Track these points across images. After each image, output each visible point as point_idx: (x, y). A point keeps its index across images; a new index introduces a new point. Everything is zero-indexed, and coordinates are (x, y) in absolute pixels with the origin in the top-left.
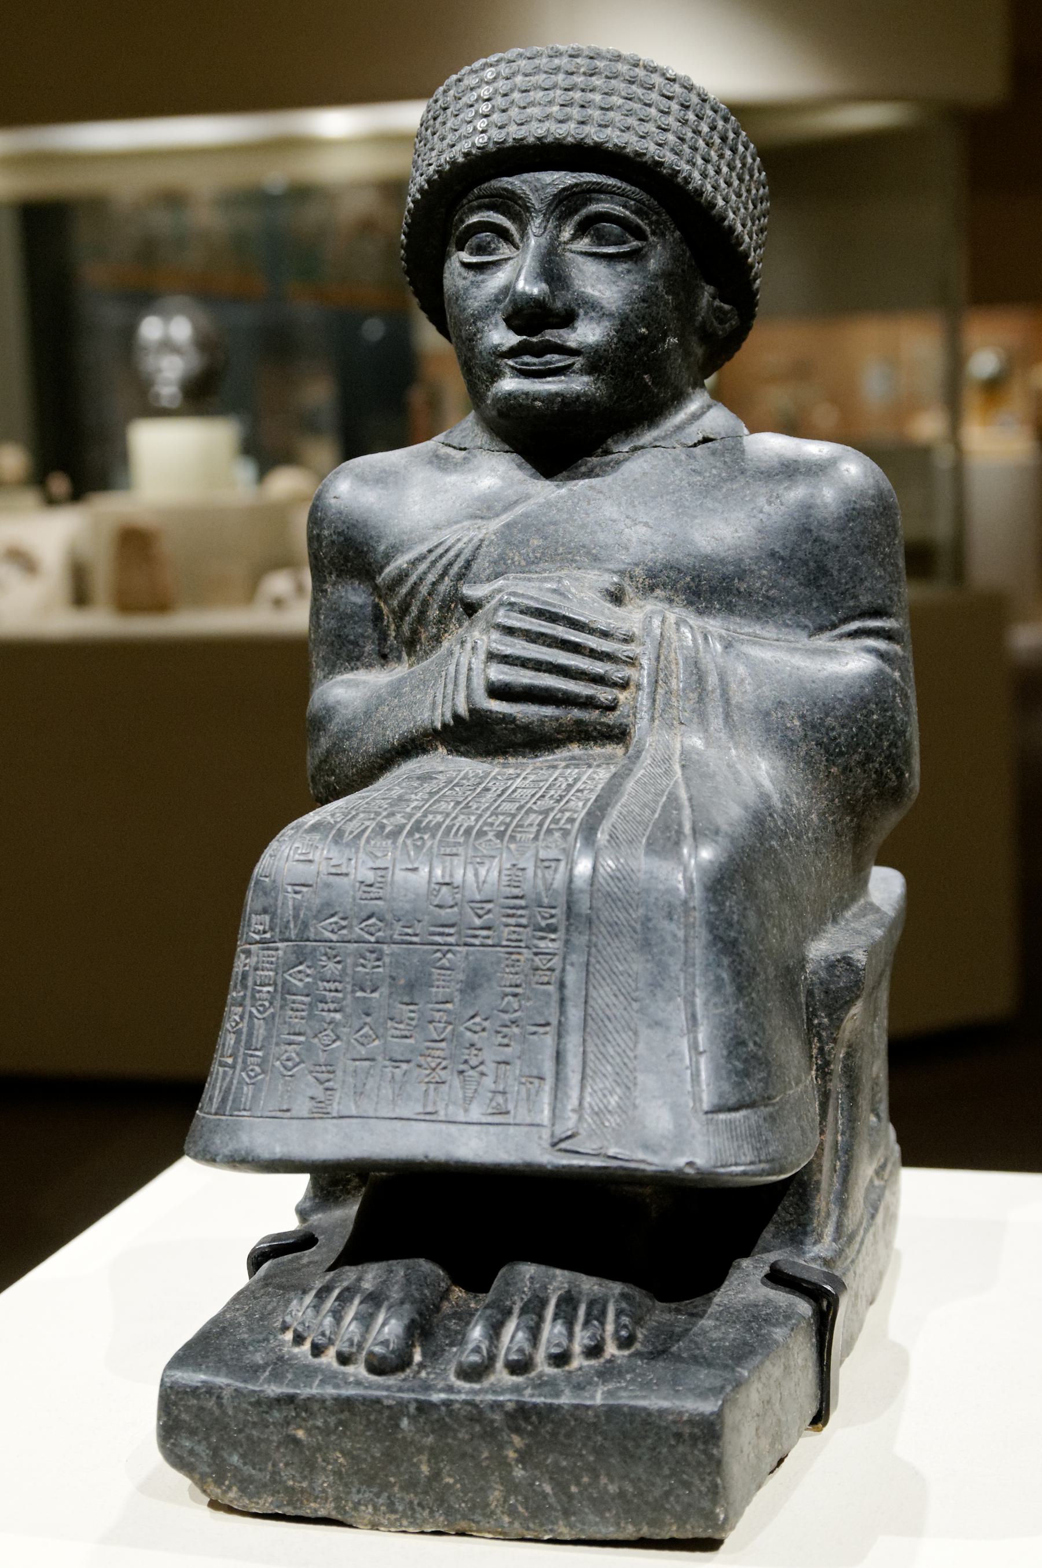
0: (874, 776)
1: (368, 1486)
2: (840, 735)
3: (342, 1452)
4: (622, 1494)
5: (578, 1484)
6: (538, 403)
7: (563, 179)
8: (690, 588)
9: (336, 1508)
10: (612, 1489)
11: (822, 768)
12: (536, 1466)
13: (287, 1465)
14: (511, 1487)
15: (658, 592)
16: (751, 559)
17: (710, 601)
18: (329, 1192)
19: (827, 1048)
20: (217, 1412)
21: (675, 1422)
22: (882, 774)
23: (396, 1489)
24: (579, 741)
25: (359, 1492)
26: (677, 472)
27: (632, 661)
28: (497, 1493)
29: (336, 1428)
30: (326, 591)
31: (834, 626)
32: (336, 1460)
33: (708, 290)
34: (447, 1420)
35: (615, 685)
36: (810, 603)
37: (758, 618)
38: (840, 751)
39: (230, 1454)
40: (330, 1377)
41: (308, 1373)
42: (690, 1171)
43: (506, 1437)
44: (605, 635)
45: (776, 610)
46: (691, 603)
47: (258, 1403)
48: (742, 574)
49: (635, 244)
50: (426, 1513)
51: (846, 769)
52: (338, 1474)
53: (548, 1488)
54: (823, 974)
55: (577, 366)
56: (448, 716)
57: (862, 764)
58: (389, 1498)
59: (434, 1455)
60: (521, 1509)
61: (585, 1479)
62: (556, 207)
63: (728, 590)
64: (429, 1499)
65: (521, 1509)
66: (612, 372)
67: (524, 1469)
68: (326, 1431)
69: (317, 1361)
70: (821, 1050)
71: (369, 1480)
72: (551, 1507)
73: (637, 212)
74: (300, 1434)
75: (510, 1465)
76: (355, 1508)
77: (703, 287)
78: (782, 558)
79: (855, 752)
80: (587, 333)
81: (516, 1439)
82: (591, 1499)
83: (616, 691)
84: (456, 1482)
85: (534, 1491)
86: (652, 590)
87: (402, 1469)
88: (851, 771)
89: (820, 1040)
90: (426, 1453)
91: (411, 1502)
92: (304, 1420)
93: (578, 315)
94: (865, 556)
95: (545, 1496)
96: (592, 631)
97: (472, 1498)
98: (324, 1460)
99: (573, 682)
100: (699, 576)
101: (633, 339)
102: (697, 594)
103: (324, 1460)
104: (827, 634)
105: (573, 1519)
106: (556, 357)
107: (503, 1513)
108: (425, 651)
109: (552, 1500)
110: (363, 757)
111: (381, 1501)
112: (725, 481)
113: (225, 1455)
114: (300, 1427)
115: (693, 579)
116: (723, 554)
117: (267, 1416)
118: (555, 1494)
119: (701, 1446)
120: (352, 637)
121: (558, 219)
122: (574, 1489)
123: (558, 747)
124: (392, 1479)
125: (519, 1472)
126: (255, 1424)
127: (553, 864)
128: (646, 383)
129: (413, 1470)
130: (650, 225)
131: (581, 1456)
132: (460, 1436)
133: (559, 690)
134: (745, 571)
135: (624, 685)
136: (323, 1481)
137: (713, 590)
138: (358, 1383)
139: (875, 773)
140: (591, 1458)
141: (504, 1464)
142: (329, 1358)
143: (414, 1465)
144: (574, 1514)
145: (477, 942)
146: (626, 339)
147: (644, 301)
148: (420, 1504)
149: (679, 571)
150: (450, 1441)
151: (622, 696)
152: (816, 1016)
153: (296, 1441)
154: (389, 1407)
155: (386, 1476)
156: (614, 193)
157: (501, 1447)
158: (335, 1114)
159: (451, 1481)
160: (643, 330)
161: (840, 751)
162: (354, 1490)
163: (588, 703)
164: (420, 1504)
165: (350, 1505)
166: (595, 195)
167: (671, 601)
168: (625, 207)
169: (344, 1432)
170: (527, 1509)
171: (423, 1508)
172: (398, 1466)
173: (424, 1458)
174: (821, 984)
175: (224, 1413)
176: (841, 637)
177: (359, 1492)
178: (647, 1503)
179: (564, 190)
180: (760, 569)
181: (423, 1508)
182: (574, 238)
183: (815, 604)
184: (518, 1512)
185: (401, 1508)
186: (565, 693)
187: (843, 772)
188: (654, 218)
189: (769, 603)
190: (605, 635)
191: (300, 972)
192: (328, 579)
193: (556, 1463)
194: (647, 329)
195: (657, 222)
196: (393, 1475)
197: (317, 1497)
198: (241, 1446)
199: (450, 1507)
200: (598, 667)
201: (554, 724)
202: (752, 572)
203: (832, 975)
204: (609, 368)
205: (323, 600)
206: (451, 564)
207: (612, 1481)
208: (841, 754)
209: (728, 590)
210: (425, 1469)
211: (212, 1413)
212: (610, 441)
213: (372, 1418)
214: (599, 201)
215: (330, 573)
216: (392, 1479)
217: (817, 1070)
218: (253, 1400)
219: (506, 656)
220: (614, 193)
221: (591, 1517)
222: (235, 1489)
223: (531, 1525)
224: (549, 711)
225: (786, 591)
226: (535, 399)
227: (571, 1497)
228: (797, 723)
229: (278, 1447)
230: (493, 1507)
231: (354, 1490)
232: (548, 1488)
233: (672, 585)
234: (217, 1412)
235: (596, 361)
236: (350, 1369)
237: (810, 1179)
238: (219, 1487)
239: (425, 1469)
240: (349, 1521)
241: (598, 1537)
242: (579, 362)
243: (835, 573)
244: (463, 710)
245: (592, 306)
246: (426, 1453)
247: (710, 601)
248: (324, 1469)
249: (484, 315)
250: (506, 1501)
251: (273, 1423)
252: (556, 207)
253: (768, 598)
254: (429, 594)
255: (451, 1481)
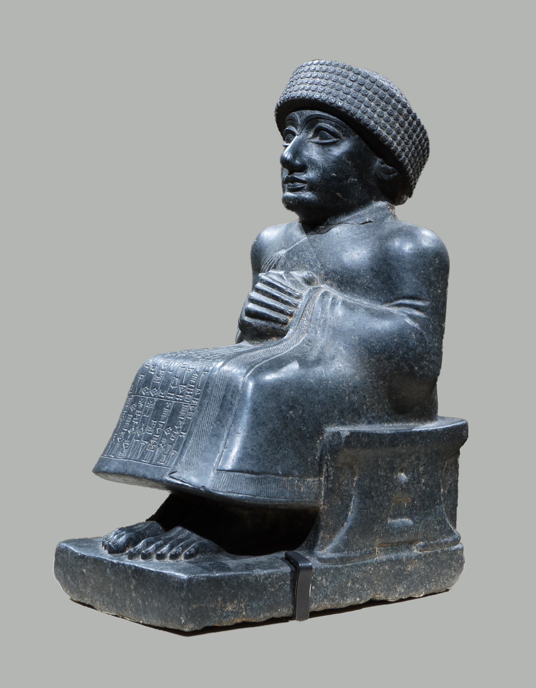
0: (395, 365)
2: (376, 346)
4: (158, 607)
6: (291, 202)
7: (308, 113)
8: (339, 281)
11: (366, 358)
14: (132, 600)
15: (328, 281)
16: (364, 270)
17: (346, 287)
19: (329, 469)
20: (66, 559)
21: (173, 582)
22: (399, 365)
24: (276, 337)
27: (296, 306)
31: (392, 301)
33: (379, 160)
35: (287, 314)
36: (383, 291)
37: (364, 295)
38: (376, 352)
42: (202, 489)
44: (290, 294)
45: (370, 293)
46: (339, 287)
48: (359, 276)
49: (335, 140)
51: (378, 360)
52: (92, 587)
53: (140, 602)
54: (330, 438)
55: (305, 188)
61: (150, 600)
62: (306, 124)
63: (353, 283)
66: (319, 190)
70: (327, 470)
72: (141, 609)
73: (336, 127)
77: (376, 159)
78: (375, 271)
79: (384, 353)
80: (310, 175)
83: (288, 317)
86: (326, 280)
88: (381, 361)
89: (327, 465)
93: (308, 167)
94: (408, 273)
96: (286, 293)
99: (273, 312)
100: (343, 276)
101: (328, 177)
102: (341, 283)
104: (388, 304)
106: (298, 183)
114: (84, 568)
115: (340, 277)
116: (353, 268)
119: (178, 592)
121: (307, 129)
123: (269, 338)
128: (339, 197)
130: (342, 132)
133: (266, 314)
134: (361, 275)
135: (291, 315)
137: (347, 282)
139: (396, 364)
145: (178, 399)
146: (325, 177)
147: (334, 162)
149: (336, 273)
151: (290, 320)
152: (326, 455)
153: (83, 573)
156: (325, 119)
159: (117, 595)
160: (334, 174)
161: (376, 352)
163: (276, 321)
166: (319, 120)
167: (332, 285)
168: (330, 124)
174: (329, 442)
176: (393, 306)
179: (308, 117)
180: (367, 275)
182: (314, 137)
183: (385, 291)
186: (268, 316)
188: (344, 129)
189: (368, 289)
190: (290, 294)
194: (336, 174)
195: (345, 131)
200: (282, 307)
202: (364, 276)
203: (333, 438)
204: (318, 189)
208: (376, 353)
209: (353, 283)
212: (328, 220)
214: (321, 122)
216: (104, 592)
217: (325, 478)
220: (325, 119)
221: (150, 615)
224: (264, 323)
225: (375, 284)
226: (290, 200)
233: (332, 279)
235: (312, 186)
237: (319, 524)
240: (95, 607)
241: (153, 624)
242: (306, 185)
243: (394, 279)
245: (312, 162)
247: (346, 287)
252: (306, 124)
253: (368, 287)
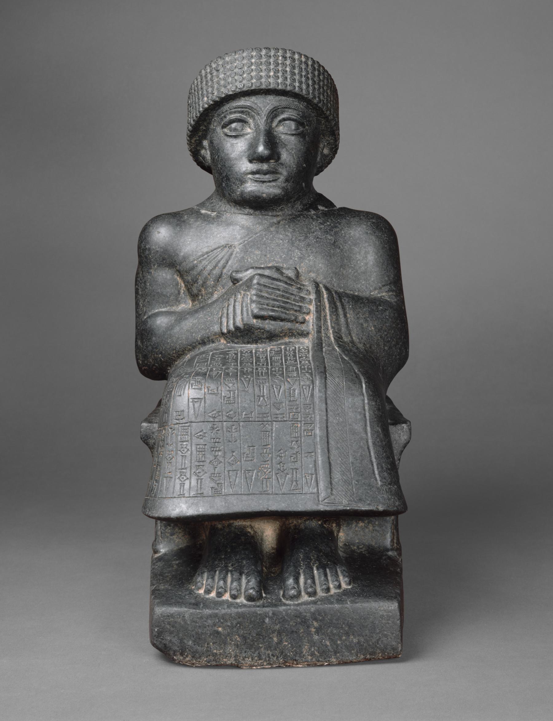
1: (250, 649)
3: (238, 635)
5: (341, 640)
9: (235, 660)
10: (355, 641)
12: (323, 634)
13: (213, 643)
14: (312, 644)
18: (171, 539)
23: (262, 649)
25: (245, 652)
26: (314, 223)
28: (306, 647)
29: (237, 625)
30: (151, 273)
32: (236, 639)
34: (286, 617)
39: (188, 641)
40: (230, 605)
41: (217, 604)
43: (311, 622)
47: (201, 618)
50: (275, 658)
52: (237, 646)
53: (328, 643)
56: (232, 327)
57: (395, 345)
58: (259, 653)
59: (279, 633)
60: (316, 653)
64: (277, 652)
65: (316, 653)
67: (318, 635)
68: (232, 627)
69: (220, 599)
71: (250, 647)
74: (220, 629)
75: (312, 635)
76: (244, 659)
81: (315, 624)
82: (346, 646)
84: (289, 644)
85: (322, 644)
87: (265, 640)
90: (276, 633)
91: (269, 654)
92: (222, 623)
95: (326, 646)
97: (295, 650)
98: (230, 640)
103: (230, 640)
105: (338, 654)
107: (308, 655)
108: (204, 299)
109: (330, 648)
110: (180, 346)
111: (255, 655)
112: (333, 227)
113: (186, 642)
114: (220, 627)
117: (206, 623)
118: (331, 645)
120: (165, 293)
122: (339, 642)
124: (261, 645)
125: (316, 637)
126: (200, 627)
127: (199, 400)
129: (270, 640)
131: (342, 627)
132: (291, 623)
136: (230, 649)
138: (245, 606)
140: (347, 629)
141: (309, 634)
142: (227, 597)
143: (270, 638)
144: (339, 653)
148: (272, 655)
150: (287, 626)
153: (218, 632)
154: (260, 615)
155: (258, 644)
157: (308, 627)
158: (223, 494)
159: (287, 644)
162: (243, 651)
164: (272, 655)
165: (242, 658)
166: (286, 110)
169: (239, 626)
170: (319, 652)
171: (274, 656)
172: (263, 639)
173: (275, 635)
175: (186, 623)
177: (245, 652)
178: (369, 645)
181: (274, 656)
184: (315, 654)
185: (264, 657)
187: (389, 349)
191: (200, 435)
192: (153, 267)
193: (332, 632)
196: (262, 644)
197: (227, 656)
198: (193, 637)
199: (286, 655)
201: (280, 330)
205: (149, 277)
206: (219, 261)
207: (355, 637)
210: (275, 639)
211: (180, 624)
213: (252, 619)
215: (154, 265)
216: (261, 645)
218: (199, 616)
219: (138, 304)
221: (346, 653)
222: (190, 656)
223: (320, 659)
227: (337, 646)
228: (373, 328)
229: (210, 636)
230: (304, 653)
231: (243, 651)
232: (328, 643)
234: (182, 623)
236: (238, 601)
238: (182, 656)
239: (275, 639)
244: (239, 324)
246: (276, 633)
248: (231, 644)
249: (240, 158)
250: (310, 650)
251: (208, 626)
254: (209, 274)
255: (287, 644)
